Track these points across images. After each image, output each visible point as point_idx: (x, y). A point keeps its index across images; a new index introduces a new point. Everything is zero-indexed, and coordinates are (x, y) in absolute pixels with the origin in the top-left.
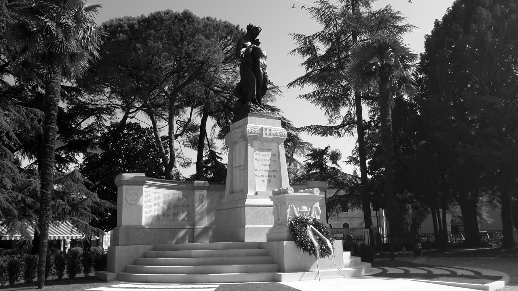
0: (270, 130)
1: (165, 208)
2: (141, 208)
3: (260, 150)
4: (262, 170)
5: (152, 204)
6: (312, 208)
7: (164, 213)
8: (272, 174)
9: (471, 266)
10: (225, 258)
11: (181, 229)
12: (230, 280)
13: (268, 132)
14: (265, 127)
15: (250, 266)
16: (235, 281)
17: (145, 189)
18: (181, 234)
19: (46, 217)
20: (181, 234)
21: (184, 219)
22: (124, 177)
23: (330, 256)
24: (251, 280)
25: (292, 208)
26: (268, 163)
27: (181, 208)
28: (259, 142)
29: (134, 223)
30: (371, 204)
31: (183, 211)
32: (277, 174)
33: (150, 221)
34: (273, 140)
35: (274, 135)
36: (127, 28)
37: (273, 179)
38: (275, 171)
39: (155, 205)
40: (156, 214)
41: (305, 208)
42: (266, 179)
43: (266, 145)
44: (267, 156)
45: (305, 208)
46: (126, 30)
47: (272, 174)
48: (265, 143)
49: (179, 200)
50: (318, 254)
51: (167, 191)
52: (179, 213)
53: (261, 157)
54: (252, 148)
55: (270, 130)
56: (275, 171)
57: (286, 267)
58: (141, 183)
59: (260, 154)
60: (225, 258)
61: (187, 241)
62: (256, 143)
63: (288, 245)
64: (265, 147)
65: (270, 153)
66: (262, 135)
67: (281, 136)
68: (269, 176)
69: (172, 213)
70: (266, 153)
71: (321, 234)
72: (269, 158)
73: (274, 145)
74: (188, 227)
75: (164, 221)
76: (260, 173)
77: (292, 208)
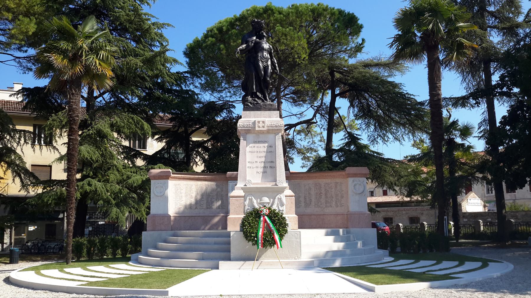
0: (263, 122)
1: (199, 197)
2: (166, 199)
3: (255, 142)
4: (256, 162)
5: (183, 195)
6: (274, 199)
7: (197, 202)
8: (268, 165)
9: (145, 274)
10: (193, 246)
11: (214, 216)
12: (190, 266)
13: (261, 125)
14: (257, 119)
15: (206, 253)
16: (178, 266)
17: (171, 183)
18: (216, 220)
19: (70, 209)
20: (216, 220)
21: (219, 207)
22: (151, 173)
23: (276, 246)
24: (200, 266)
25: (251, 200)
26: (264, 154)
27: (215, 197)
28: (254, 135)
29: (160, 212)
30: (504, 183)
31: (217, 200)
32: (272, 165)
33: (182, 209)
34: (268, 132)
35: (268, 127)
36: (216, 32)
37: (269, 170)
38: (272, 162)
39: (186, 196)
40: (188, 203)
41: (266, 200)
42: (262, 170)
43: (262, 137)
44: (263, 148)
45: (266, 200)
46: (215, 34)
47: (268, 165)
48: (261, 135)
49: (213, 190)
50: (260, 245)
51: (199, 183)
52: (212, 203)
53: (256, 149)
54: (245, 142)
55: (263, 122)
56: (272, 162)
57: (232, 255)
58: (166, 177)
59: (254, 147)
60: (193, 246)
61: (220, 228)
62: (250, 137)
63: (235, 235)
64: (260, 140)
65: (266, 145)
66: (255, 128)
67: (276, 127)
68: (265, 167)
69: (205, 202)
70: (262, 145)
71: (271, 225)
72: (265, 150)
73: (271, 136)
74: (222, 215)
75: (196, 210)
76: (255, 165)
77: (251, 200)
